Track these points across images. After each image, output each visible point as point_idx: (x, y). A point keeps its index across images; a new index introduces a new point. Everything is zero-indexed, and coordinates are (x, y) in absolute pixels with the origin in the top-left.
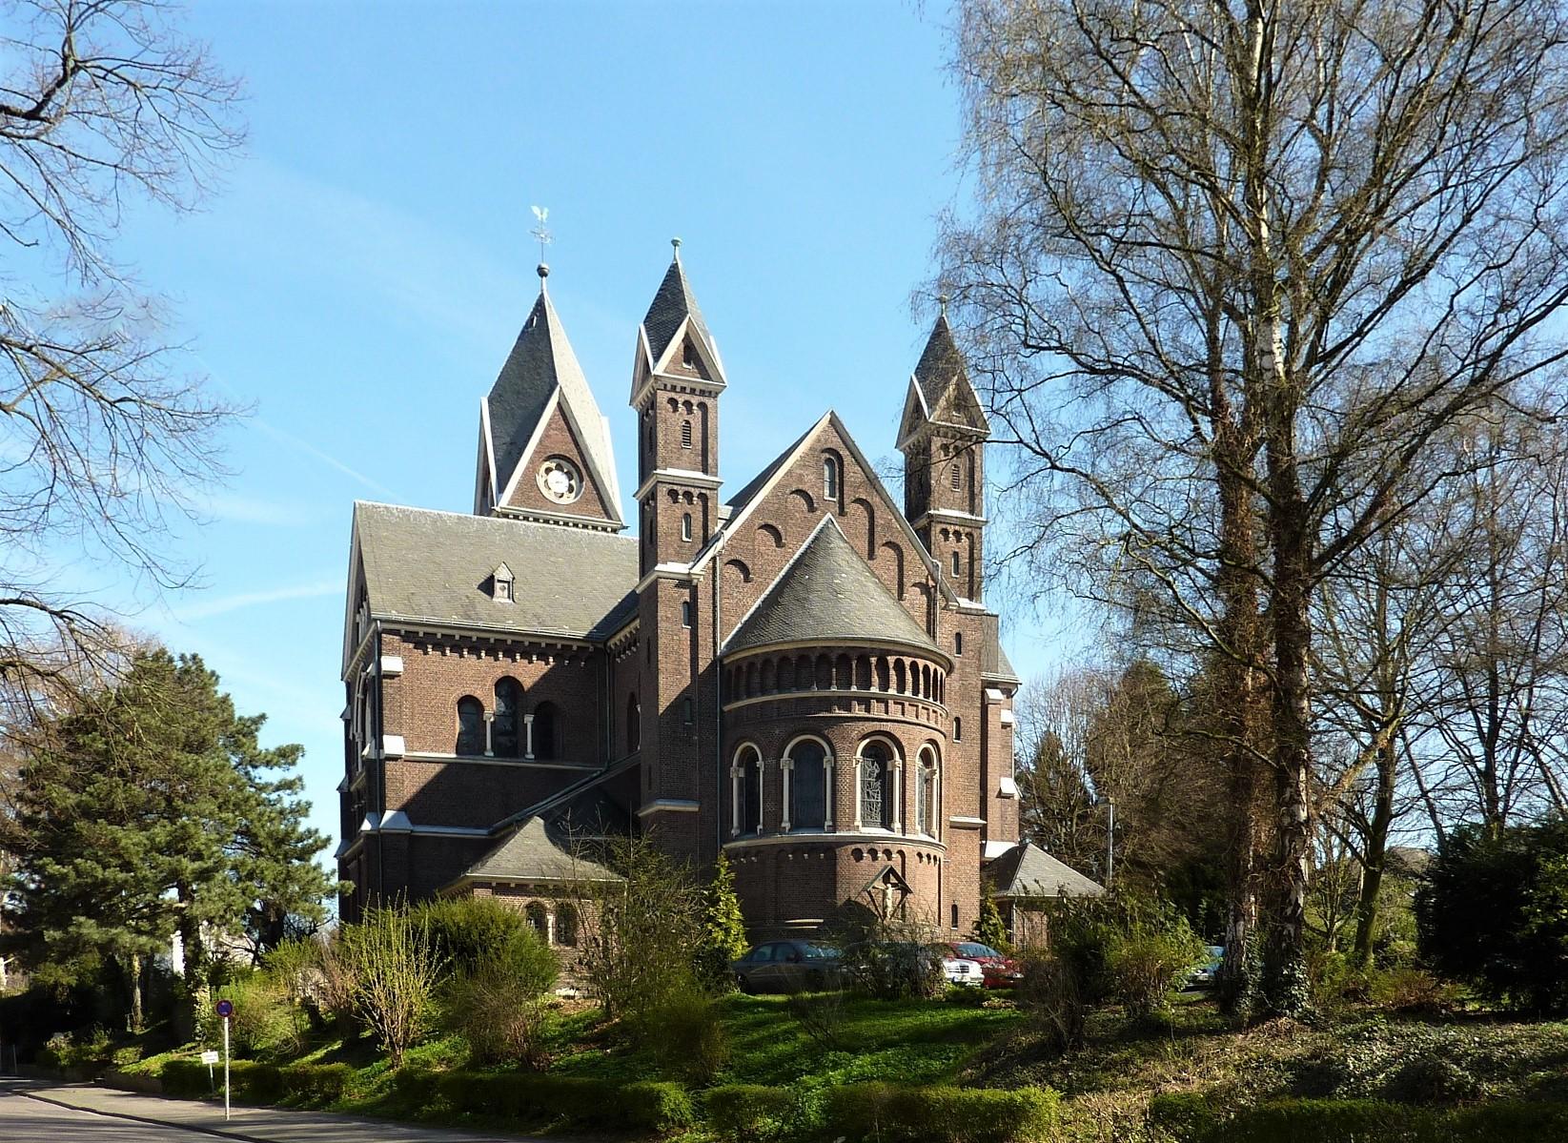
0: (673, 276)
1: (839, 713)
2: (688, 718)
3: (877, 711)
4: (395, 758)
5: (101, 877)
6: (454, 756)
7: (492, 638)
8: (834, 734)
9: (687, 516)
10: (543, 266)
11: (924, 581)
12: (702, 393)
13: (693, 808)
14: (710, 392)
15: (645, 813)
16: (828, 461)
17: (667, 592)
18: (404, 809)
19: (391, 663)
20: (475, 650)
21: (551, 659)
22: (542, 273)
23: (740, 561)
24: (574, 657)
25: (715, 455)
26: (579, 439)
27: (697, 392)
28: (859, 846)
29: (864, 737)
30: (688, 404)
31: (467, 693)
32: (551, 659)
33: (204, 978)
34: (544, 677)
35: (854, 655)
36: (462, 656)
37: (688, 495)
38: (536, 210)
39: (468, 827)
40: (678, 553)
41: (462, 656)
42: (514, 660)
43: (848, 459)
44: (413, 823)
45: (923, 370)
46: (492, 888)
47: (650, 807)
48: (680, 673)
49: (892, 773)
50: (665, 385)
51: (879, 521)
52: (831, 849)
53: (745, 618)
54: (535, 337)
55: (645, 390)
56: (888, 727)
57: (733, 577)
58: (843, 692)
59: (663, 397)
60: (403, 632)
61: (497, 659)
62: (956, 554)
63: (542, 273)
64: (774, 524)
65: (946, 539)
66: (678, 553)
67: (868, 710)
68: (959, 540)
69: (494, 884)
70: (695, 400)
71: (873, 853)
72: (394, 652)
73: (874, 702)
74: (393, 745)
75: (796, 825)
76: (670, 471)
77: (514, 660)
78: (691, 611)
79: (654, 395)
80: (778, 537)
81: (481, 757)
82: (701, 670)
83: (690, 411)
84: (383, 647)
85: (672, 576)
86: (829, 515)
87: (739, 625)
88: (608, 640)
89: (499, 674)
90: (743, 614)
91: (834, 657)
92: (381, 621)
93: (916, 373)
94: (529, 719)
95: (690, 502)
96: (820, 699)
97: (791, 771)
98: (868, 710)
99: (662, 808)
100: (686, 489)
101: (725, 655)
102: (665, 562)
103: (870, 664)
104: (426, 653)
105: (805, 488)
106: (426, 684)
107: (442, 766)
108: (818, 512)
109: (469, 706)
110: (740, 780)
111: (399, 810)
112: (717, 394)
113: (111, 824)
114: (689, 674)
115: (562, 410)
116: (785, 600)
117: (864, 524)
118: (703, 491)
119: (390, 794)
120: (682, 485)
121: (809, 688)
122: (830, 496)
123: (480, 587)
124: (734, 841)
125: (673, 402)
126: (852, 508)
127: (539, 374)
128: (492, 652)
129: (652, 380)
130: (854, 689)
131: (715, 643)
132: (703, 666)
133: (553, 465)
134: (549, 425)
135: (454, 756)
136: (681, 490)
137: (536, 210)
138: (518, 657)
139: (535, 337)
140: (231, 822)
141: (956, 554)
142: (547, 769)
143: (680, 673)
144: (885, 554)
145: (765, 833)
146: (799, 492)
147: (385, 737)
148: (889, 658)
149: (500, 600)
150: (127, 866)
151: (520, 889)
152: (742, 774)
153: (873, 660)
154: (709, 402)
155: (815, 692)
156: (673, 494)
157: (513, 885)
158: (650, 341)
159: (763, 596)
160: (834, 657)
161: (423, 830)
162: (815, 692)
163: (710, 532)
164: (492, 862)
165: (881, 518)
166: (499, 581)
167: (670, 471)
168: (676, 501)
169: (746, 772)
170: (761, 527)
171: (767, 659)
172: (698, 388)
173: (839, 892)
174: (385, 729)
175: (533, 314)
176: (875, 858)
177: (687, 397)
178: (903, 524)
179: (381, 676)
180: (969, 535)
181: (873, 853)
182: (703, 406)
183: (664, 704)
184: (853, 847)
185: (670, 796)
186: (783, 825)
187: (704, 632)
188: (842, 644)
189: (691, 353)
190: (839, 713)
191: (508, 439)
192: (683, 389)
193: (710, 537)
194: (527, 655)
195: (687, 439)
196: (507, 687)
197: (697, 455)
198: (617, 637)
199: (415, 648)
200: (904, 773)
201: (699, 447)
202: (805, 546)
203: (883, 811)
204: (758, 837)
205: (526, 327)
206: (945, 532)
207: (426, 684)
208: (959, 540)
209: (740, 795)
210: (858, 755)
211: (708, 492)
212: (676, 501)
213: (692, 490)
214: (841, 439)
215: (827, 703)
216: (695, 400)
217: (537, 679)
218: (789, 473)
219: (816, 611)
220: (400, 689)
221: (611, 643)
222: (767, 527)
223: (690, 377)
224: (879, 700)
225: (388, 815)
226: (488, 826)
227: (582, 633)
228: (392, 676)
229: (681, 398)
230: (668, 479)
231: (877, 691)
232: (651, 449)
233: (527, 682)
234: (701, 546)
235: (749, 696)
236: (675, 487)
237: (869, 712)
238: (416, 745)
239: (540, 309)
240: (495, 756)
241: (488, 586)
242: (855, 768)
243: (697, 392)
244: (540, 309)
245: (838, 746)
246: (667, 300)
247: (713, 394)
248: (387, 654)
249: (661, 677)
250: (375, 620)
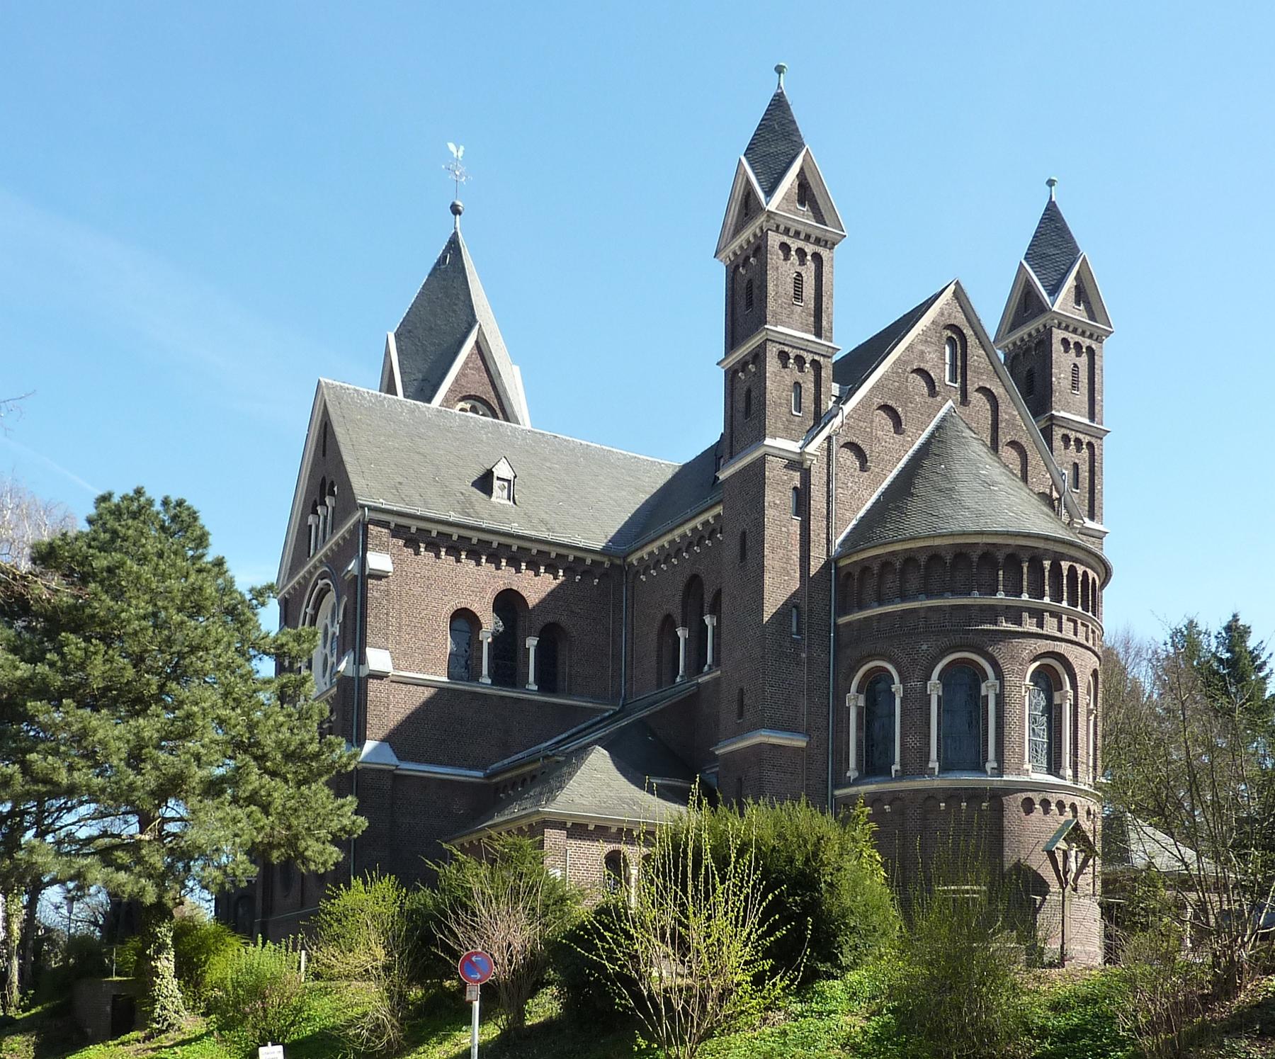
1: (1005, 626)
2: (794, 630)
3: (1050, 626)
4: (380, 676)
5: (65, 781)
6: (446, 679)
8: (1000, 651)
9: (797, 386)
10: (458, 203)
11: (1048, 491)
12: (818, 241)
13: (800, 742)
15: (722, 751)
16: (950, 339)
17: (775, 470)
18: (394, 739)
19: (378, 561)
20: (474, 555)
21: (561, 573)
22: (455, 210)
23: (989, 390)
24: (587, 573)
27: (812, 240)
28: (1030, 795)
29: (1034, 660)
30: (801, 253)
32: (561, 573)
34: (552, 594)
35: (1025, 556)
36: (458, 561)
37: (800, 360)
38: (452, 147)
39: (461, 767)
40: (786, 429)
41: (458, 561)
42: (518, 571)
43: (972, 340)
45: (1033, 255)
46: (567, 830)
48: (788, 574)
49: (1060, 706)
50: (778, 227)
51: (1003, 416)
52: (997, 796)
55: (747, 234)
56: (1062, 648)
57: (848, 463)
58: (1012, 601)
59: (774, 240)
60: (393, 525)
62: (1076, 466)
63: (455, 210)
64: (894, 405)
66: (786, 429)
68: (1079, 450)
70: (810, 249)
71: (1046, 804)
72: (382, 548)
73: (1026, 615)
74: (378, 659)
75: (946, 768)
76: (780, 329)
81: (475, 684)
82: (813, 572)
83: (802, 262)
85: (782, 453)
86: (950, 403)
87: (854, 522)
88: (629, 555)
89: (501, 586)
90: (859, 509)
91: (1001, 557)
93: (1025, 258)
94: (532, 643)
95: (801, 370)
96: (982, 608)
97: (939, 698)
98: (1040, 625)
100: (798, 352)
102: (774, 437)
103: (1043, 569)
104: (417, 553)
105: (926, 367)
106: (417, 590)
107: (432, 691)
108: (939, 398)
109: (464, 620)
110: (859, 710)
111: (383, 740)
112: (834, 244)
114: (798, 575)
115: (480, 347)
116: (920, 487)
117: (986, 418)
118: (817, 358)
119: (372, 720)
120: (794, 347)
122: (950, 381)
123: (474, 484)
124: (850, 785)
125: (785, 247)
126: (976, 398)
127: (454, 311)
128: (494, 559)
129: (763, 218)
130: (1025, 597)
131: (828, 541)
132: (815, 566)
133: (468, 406)
134: (466, 363)
135: (446, 679)
136: (793, 353)
137: (452, 147)
138: (523, 566)
140: (233, 722)
141: (1076, 466)
142: (554, 704)
143: (788, 574)
144: (1010, 455)
145: (903, 775)
146: (920, 371)
147: (367, 649)
148: (1044, 562)
152: (862, 703)
153: (1047, 564)
154: (825, 253)
155: (976, 599)
156: (783, 356)
157: (591, 827)
158: (756, 174)
160: (1001, 557)
161: (409, 767)
162: (976, 599)
164: (562, 797)
165: (1006, 413)
166: (498, 478)
167: (780, 329)
169: (867, 700)
170: (880, 408)
171: (886, 564)
173: (1007, 852)
174: (369, 640)
176: (1046, 812)
177: (801, 244)
179: (366, 576)
180: (1090, 445)
181: (1046, 804)
182: (817, 258)
184: (1024, 795)
185: (775, 727)
186: (930, 765)
187: (817, 525)
189: (805, 193)
190: (1005, 626)
191: (420, 376)
192: (797, 234)
194: (533, 566)
195: (798, 295)
196: (508, 602)
198: (648, 549)
201: (812, 305)
203: (1049, 753)
204: (892, 780)
205: (438, 263)
206: (1066, 439)
208: (1079, 450)
209: (859, 728)
211: (822, 360)
212: (785, 366)
213: (804, 354)
214: (966, 316)
215: (993, 613)
216: (810, 249)
217: (543, 595)
218: (910, 348)
220: (387, 592)
221: (634, 559)
222: (886, 408)
223: (803, 217)
224: (1053, 614)
225: (369, 745)
226: (484, 768)
227: (599, 546)
228: (380, 576)
229: (794, 245)
230: (781, 338)
232: (750, 303)
233: (533, 598)
234: (812, 423)
236: (786, 349)
240: (493, 684)
241: (485, 483)
243: (812, 240)
245: (1006, 667)
246: (773, 131)
247: (830, 244)
248: (374, 550)
249: (767, 576)
250: (363, 507)
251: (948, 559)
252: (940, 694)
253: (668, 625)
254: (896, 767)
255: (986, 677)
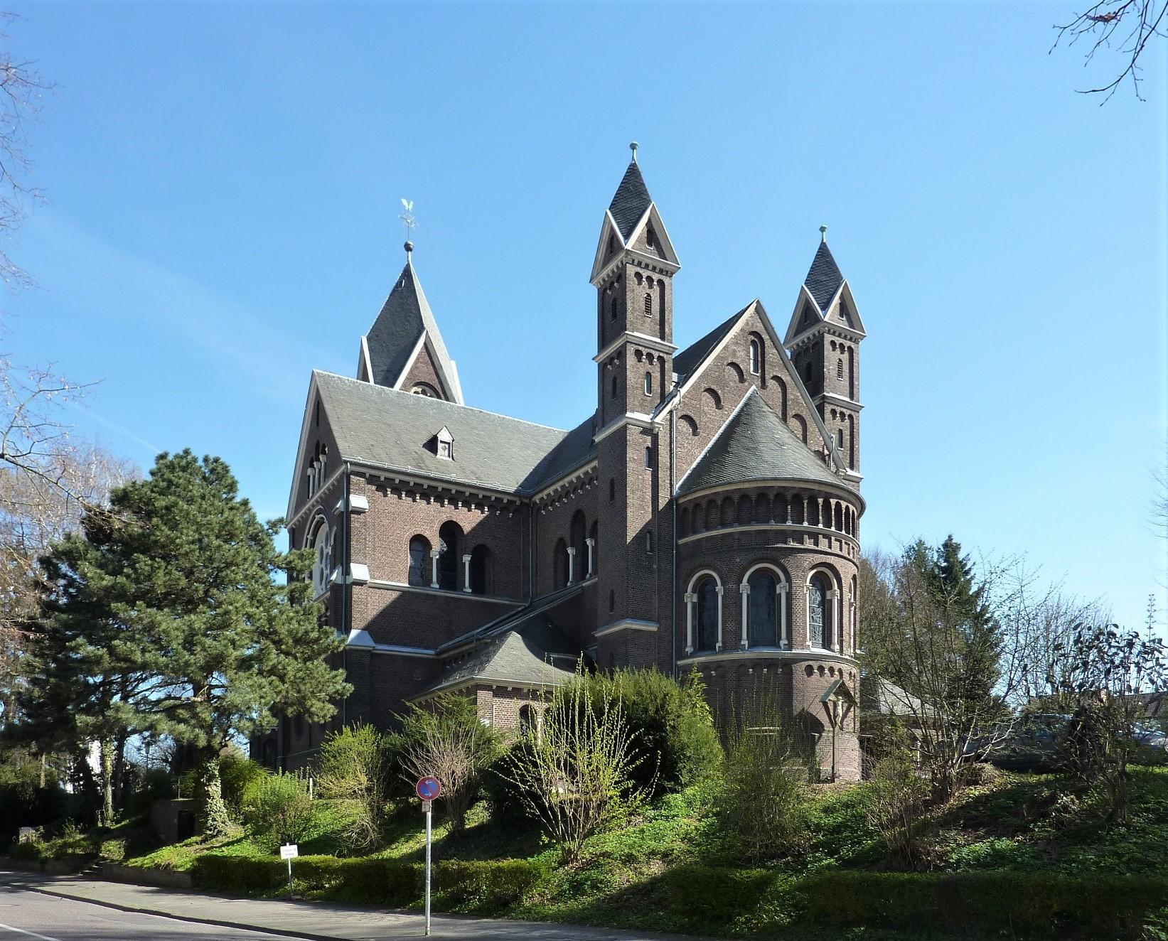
0: (633, 172)
1: (793, 544)
4: (361, 583)
6: (407, 585)
7: (440, 486)
8: (789, 562)
9: (648, 375)
12: (661, 271)
14: (667, 272)
16: (753, 342)
17: (633, 435)
18: (367, 628)
19: (358, 501)
21: (486, 509)
22: (408, 248)
24: (505, 509)
25: (670, 324)
26: (440, 373)
28: (811, 663)
29: (812, 568)
30: (650, 279)
31: (418, 533)
32: (486, 509)
33: (216, 772)
34: (481, 524)
35: (805, 495)
37: (650, 356)
38: (404, 202)
39: (419, 647)
40: (641, 405)
42: (456, 508)
43: (768, 343)
44: (376, 642)
47: (614, 626)
48: (644, 509)
49: (831, 601)
50: (633, 261)
51: (790, 396)
52: (788, 664)
53: (694, 466)
54: (403, 295)
55: (612, 266)
56: (831, 560)
57: (684, 429)
58: (797, 527)
59: (631, 270)
60: (367, 475)
61: (442, 505)
62: (841, 431)
63: (408, 248)
64: (716, 389)
65: (834, 418)
66: (641, 405)
67: (816, 544)
68: (843, 420)
69: (494, 687)
70: (656, 277)
71: (821, 669)
72: (361, 491)
74: (359, 571)
75: (753, 644)
76: (636, 334)
77: (456, 508)
78: (652, 456)
79: (624, 267)
80: (718, 401)
82: (661, 507)
83: (651, 287)
84: (352, 487)
85: (638, 423)
86: (754, 387)
87: (689, 472)
90: (692, 462)
91: (789, 496)
92: (350, 464)
93: (805, 284)
94: (467, 559)
95: (651, 363)
96: (776, 532)
97: (748, 596)
98: (816, 544)
99: (629, 626)
101: (679, 496)
102: (633, 411)
103: (818, 504)
104: (385, 495)
105: (737, 361)
106: (386, 522)
107: (398, 593)
108: (746, 384)
109: (419, 542)
110: (694, 604)
111: (364, 629)
112: (672, 274)
113: (148, 606)
114: (650, 510)
116: (734, 447)
120: (646, 347)
121: (767, 522)
125: (638, 276)
127: (409, 321)
128: (439, 499)
129: (622, 255)
130: (806, 524)
131: (671, 485)
132: (662, 503)
133: (420, 390)
135: (407, 585)
137: (404, 202)
139: (403, 295)
141: (841, 431)
144: (796, 424)
145: (724, 649)
146: (733, 364)
147: (352, 564)
149: (442, 457)
150: (164, 649)
151: (516, 692)
152: (695, 600)
153: (820, 501)
154: (666, 280)
155: (773, 526)
156: (638, 354)
157: (510, 689)
159: (706, 449)
160: (789, 496)
161: (383, 648)
162: (773, 526)
163: (666, 390)
166: (441, 442)
167: (636, 334)
168: (640, 361)
169: (699, 597)
171: (727, 497)
172: (659, 266)
173: (795, 703)
175: (402, 277)
178: (807, 401)
179: (349, 512)
181: (821, 669)
182: (661, 283)
183: (631, 534)
184: (807, 663)
185: (636, 617)
186: (742, 643)
187: (663, 474)
188: (796, 485)
189: (652, 236)
190: (793, 544)
191: (386, 368)
192: (647, 266)
193: (667, 393)
194: (467, 504)
195: (648, 310)
196: (450, 530)
197: (656, 324)
198: (546, 492)
199: (376, 490)
200: (841, 601)
201: (658, 317)
202: (737, 410)
203: (823, 634)
204: (716, 654)
207: (386, 522)
208: (843, 420)
209: (693, 617)
210: (808, 583)
211: (665, 356)
212: (640, 361)
213: (653, 352)
214: (764, 325)
215: (784, 536)
216: (656, 277)
217: (474, 525)
218: (726, 348)
219: (767, 458)
220: (365, 524)
221: (537, 499)
222: (710, 391)
223: (650, 254)
224: (825, 536)
227: (512, 489)
228: (359, 512)
229: (645, 273)
231: (822, 527)
232: (614, 316)
235: (708, 529)
237: (817, 546)
238: (377, 574)
239: (407, 274)
240: (440, 588)
241: (432, 445)
242: (806, 597)
243: (657, 271)
244: (407, 274)
245: (793, 573)
246: (629, 191)
247: (669, 274)
249: (629, 510)
250: (346, 462)
251: (754, 498)
252: (749, 593)
253: (561, 545)
254: (719, 644)
255: (779, 580)
